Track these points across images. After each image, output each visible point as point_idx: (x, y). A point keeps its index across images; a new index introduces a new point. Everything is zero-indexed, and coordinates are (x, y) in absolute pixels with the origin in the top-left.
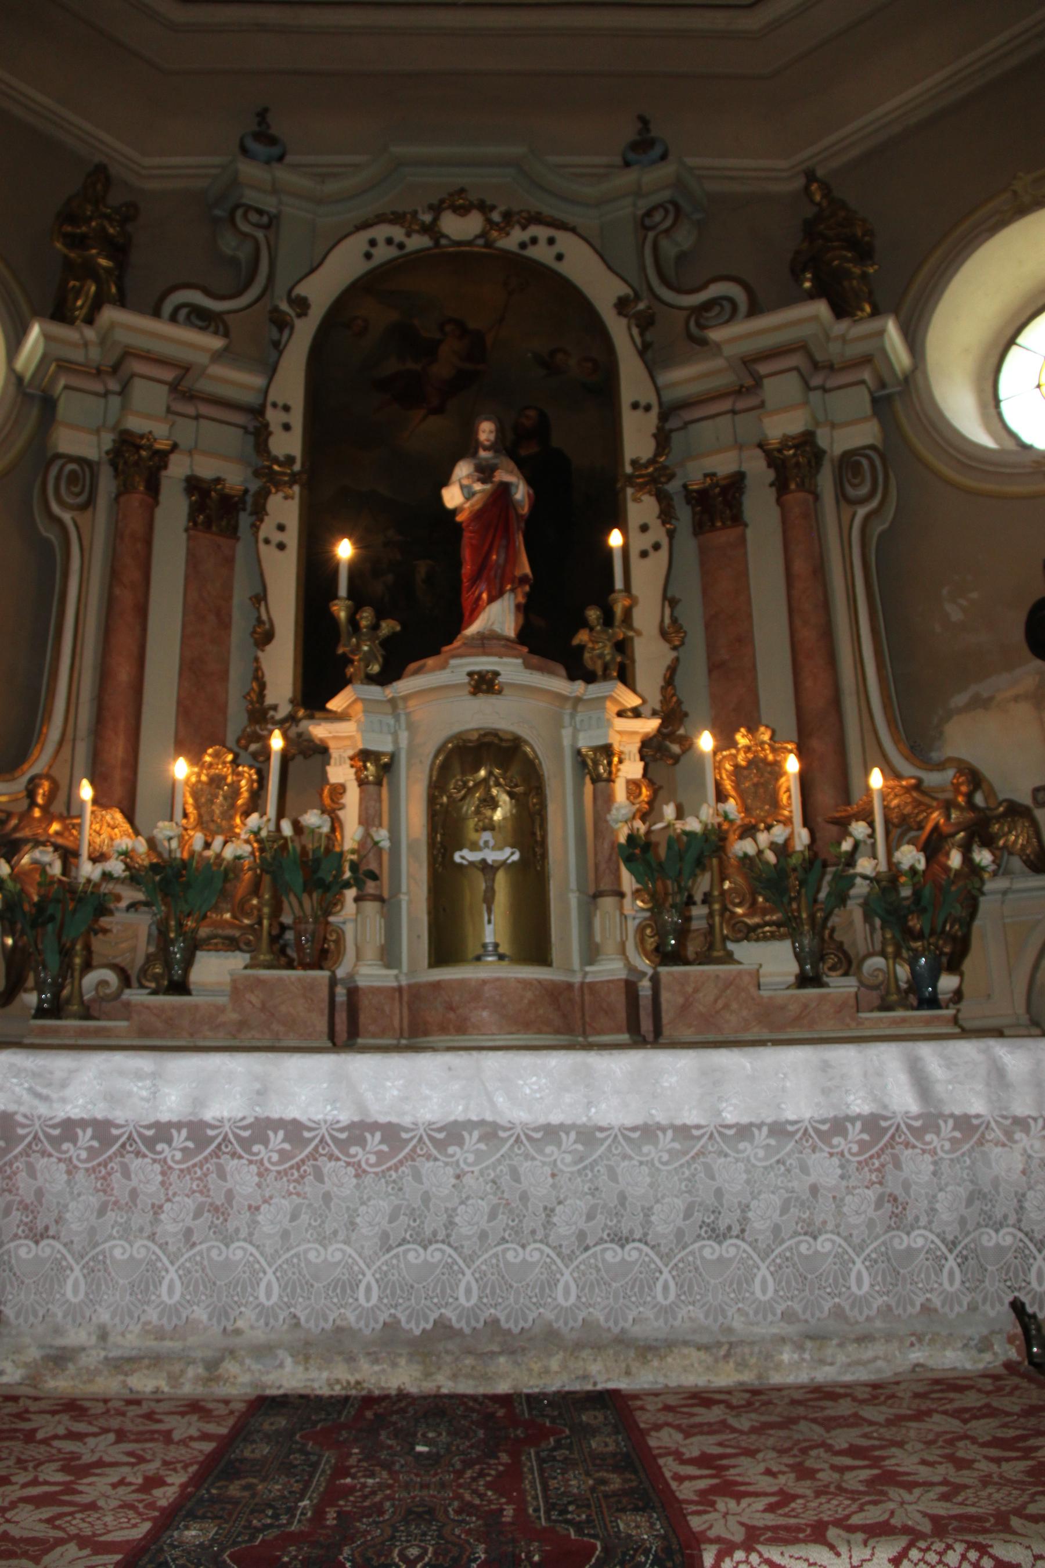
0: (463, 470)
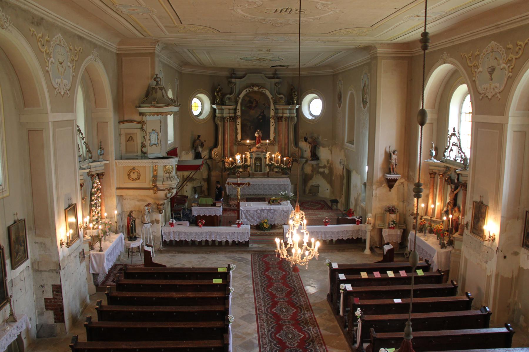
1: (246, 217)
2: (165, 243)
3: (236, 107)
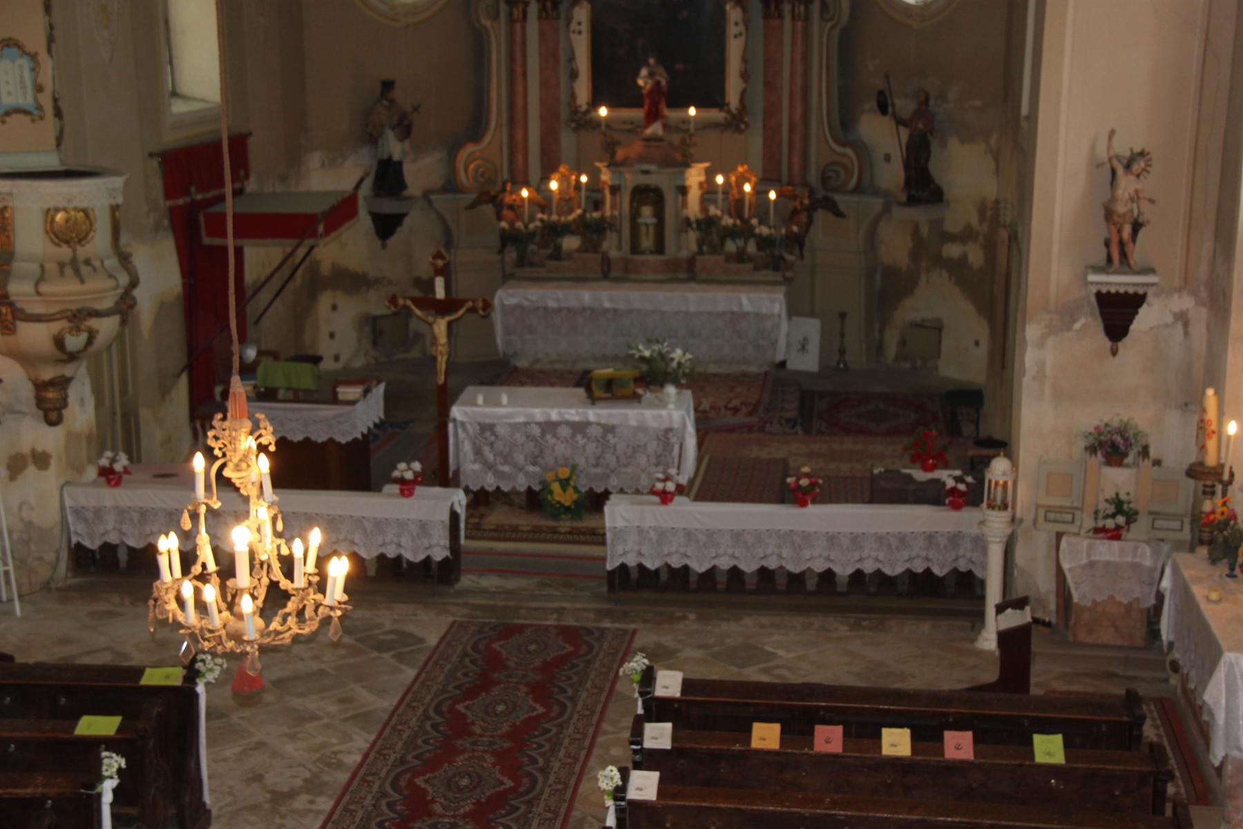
0: (644, 72)
1: (478, 452)
2: (81, 557)
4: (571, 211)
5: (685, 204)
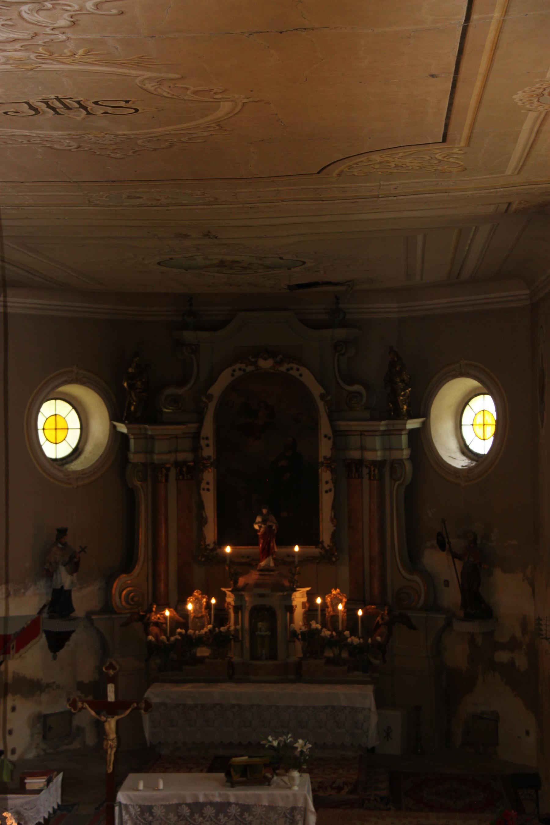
0: (259, 519)
3: (200, 428)
4: (202, 627)
5: (292, 620)
